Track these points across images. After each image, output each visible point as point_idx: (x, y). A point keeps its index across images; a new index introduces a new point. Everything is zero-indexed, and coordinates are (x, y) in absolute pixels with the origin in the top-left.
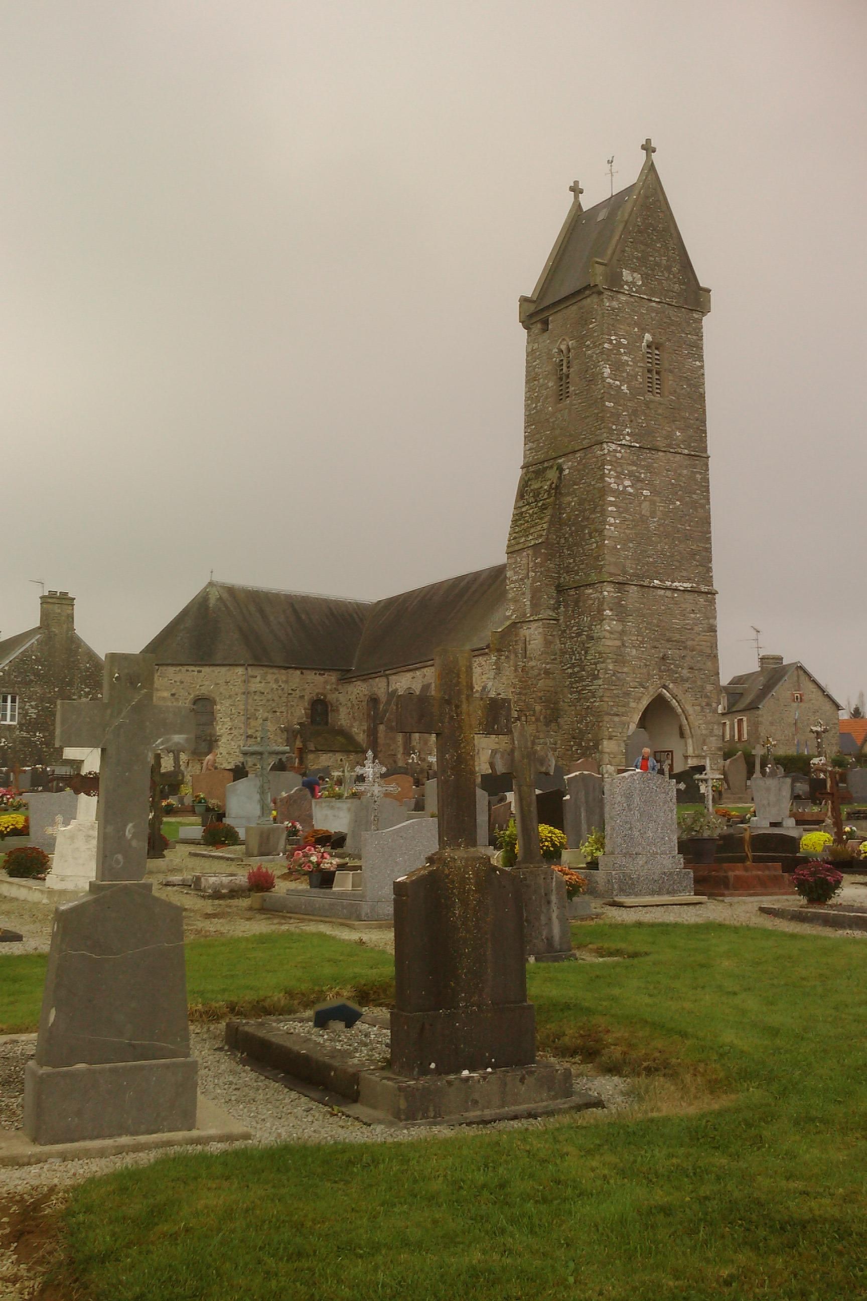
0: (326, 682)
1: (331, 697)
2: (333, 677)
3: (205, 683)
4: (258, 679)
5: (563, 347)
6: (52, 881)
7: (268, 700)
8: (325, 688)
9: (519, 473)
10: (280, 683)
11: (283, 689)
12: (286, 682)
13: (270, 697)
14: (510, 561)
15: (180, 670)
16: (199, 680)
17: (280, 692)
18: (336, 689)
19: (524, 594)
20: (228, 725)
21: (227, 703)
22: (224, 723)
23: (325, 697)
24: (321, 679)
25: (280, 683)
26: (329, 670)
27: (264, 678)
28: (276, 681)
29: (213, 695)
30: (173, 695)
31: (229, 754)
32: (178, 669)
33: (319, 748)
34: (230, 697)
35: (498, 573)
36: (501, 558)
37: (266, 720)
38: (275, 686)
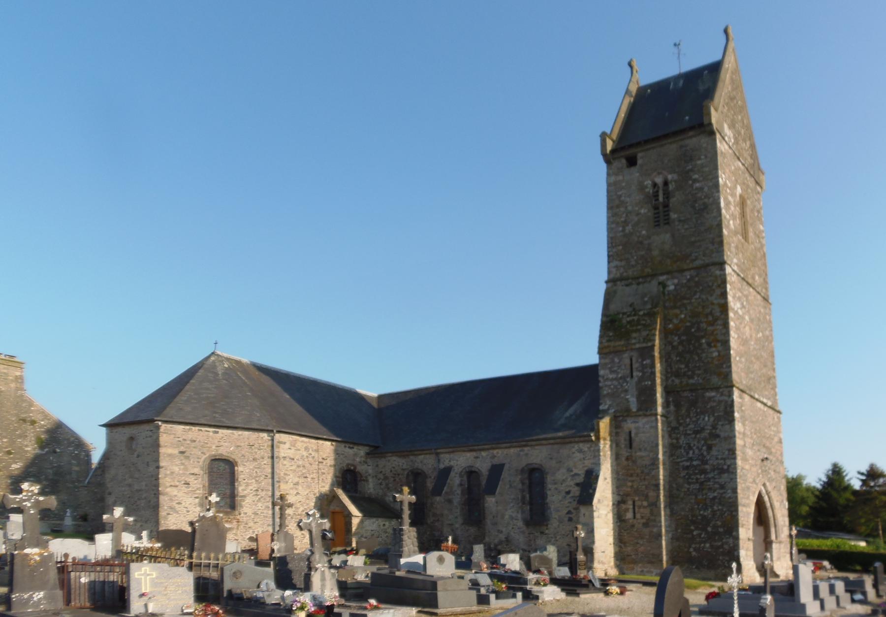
0: (355, 455)
1: (361, 468)
2: (362, 451)
3: (222, 443)
4: (287, 446)
5: (659, 180)
6: (240, 580)
7: (299, 466)
8: (354, 460)
9: (604, 287)
10: (310, 451)
11: (313, 457)
12: (317, 451)
13: (300, 463)
14: (603, 361)
15: (189, 429)
16: (216, 441)
17: (310, 459)
18: (366, 462)
19: (626, 391)
20: (254, 486)
21: (251, 465)
22: (247, 485)
23: (355, 468)
24: (351, 451)
25: (310, 451)
26: (358, 444)
27: (293, 444)
28: (306, 449)
29: (233, 457)
30: (182, 452)
31: (256, 514)
32: (188, 427)
33: (6, 578)
34: (255, 460)
35: (586, 374)
36: (592, 358)
37: (297, 484)
38: (305, 454)
